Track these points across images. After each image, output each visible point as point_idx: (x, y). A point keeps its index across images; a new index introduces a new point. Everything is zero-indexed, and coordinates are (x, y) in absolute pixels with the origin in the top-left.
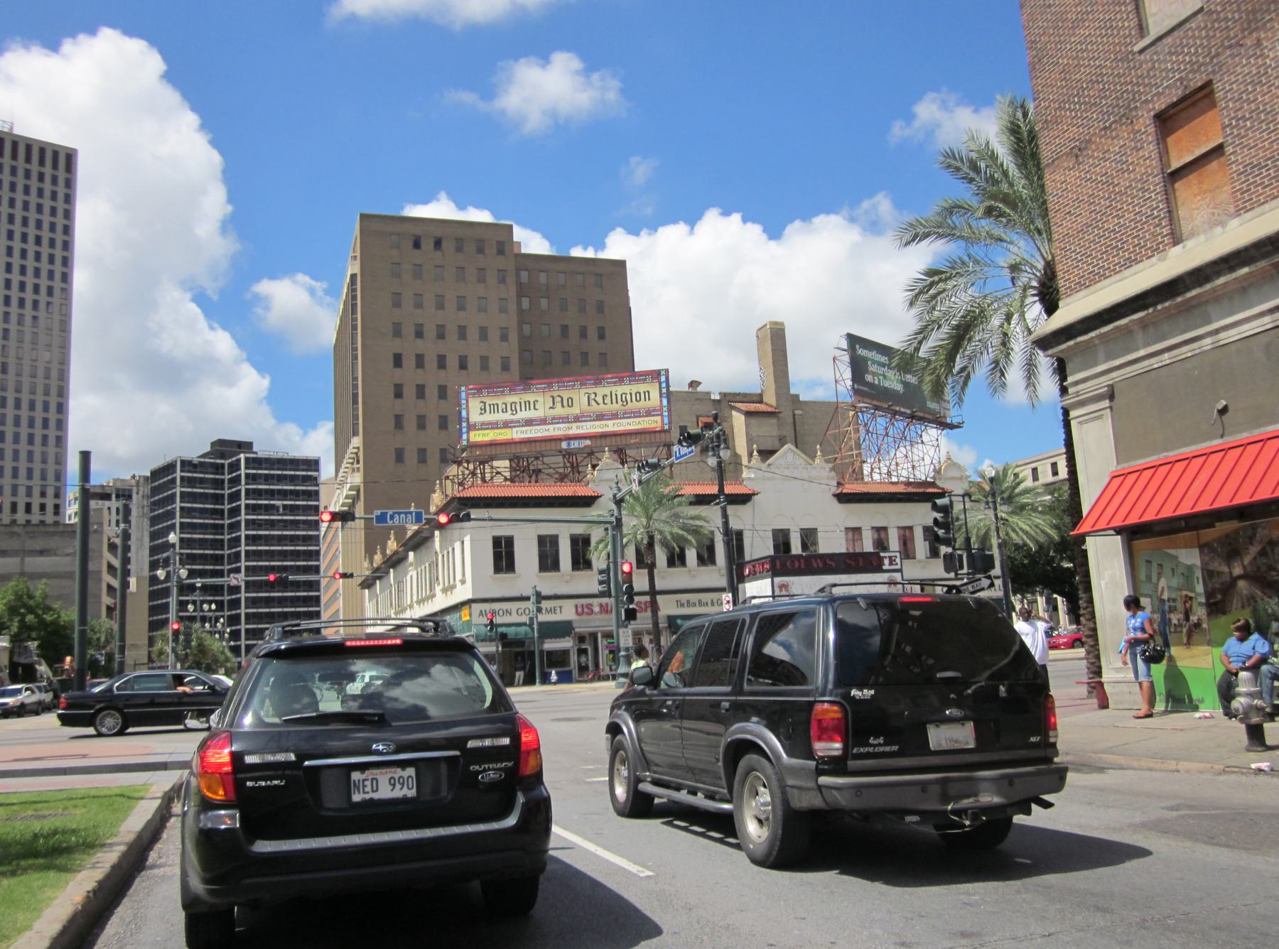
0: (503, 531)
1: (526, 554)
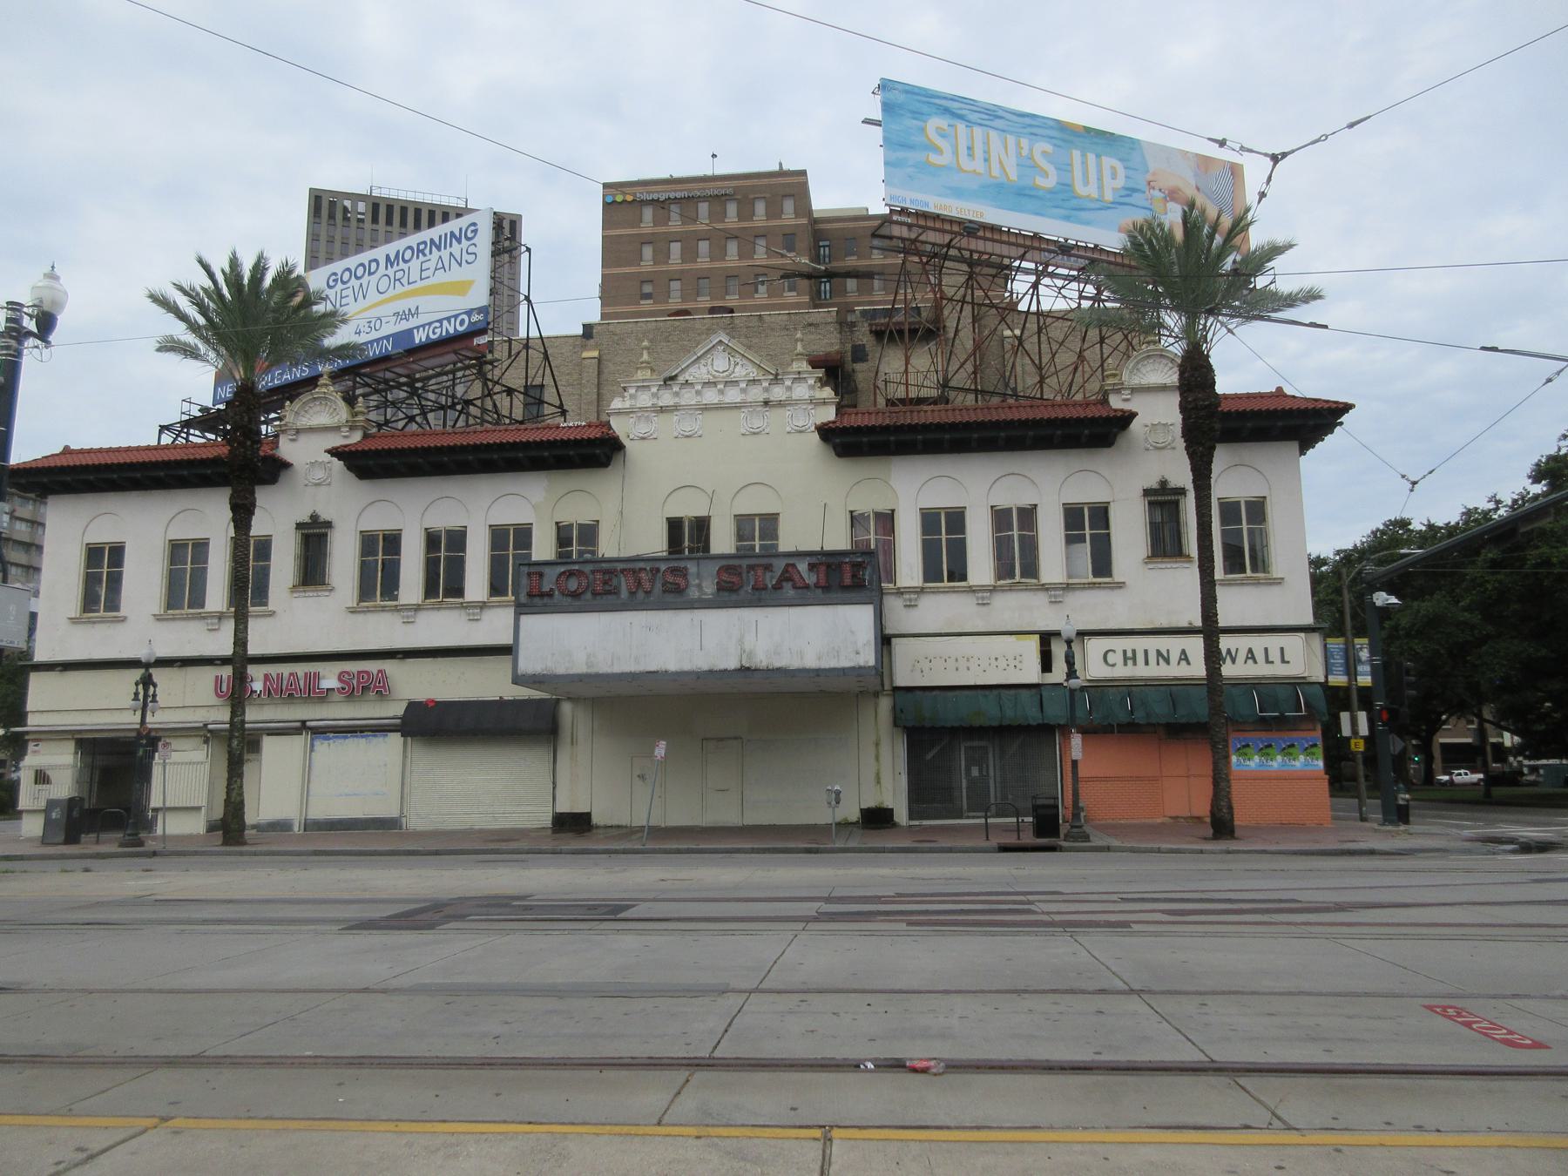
0: (103, 533)
1: (144, 580)
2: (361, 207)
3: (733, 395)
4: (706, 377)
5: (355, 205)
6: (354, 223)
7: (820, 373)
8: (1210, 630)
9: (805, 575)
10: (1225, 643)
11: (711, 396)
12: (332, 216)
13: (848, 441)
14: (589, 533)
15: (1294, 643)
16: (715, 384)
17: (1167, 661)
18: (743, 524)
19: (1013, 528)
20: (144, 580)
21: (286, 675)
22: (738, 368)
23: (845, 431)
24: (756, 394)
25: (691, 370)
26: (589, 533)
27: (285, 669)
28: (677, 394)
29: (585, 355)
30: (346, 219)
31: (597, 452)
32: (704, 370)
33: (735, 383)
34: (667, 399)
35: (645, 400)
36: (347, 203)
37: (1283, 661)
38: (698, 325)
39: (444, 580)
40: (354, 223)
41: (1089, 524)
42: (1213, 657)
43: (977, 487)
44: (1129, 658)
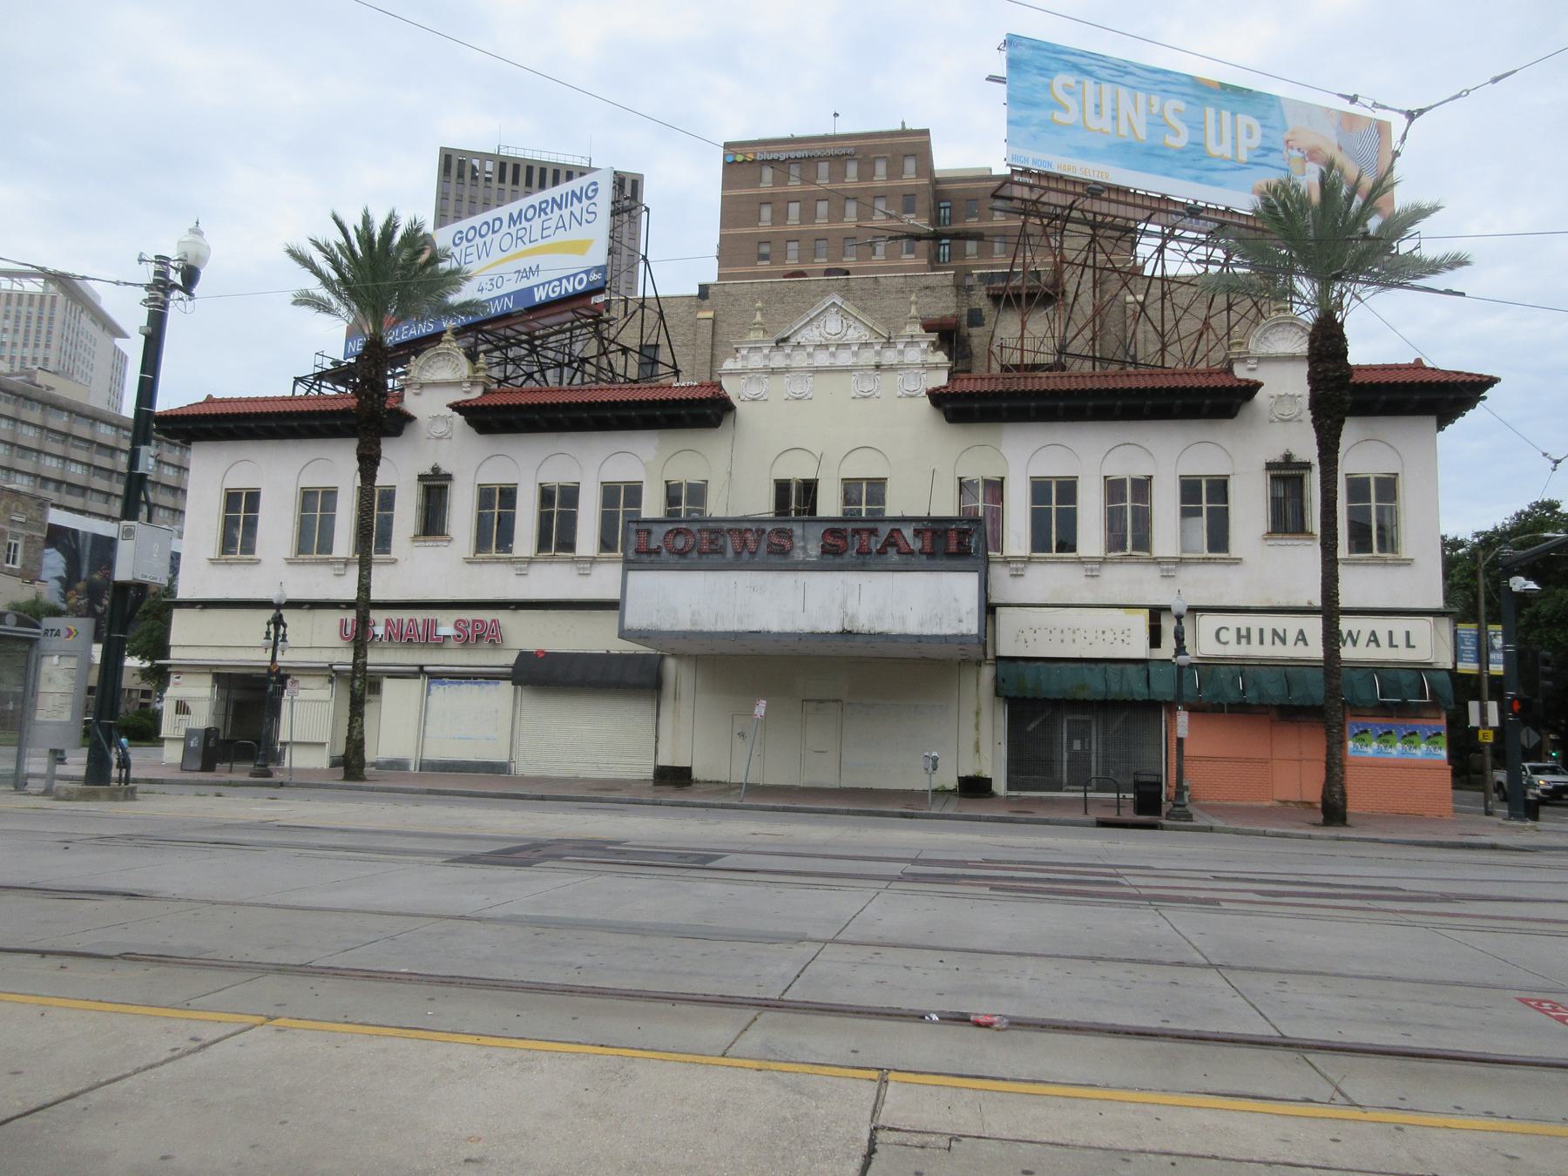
0: (241, 480)
1: (277, 524)
2: (489, 166)
3: (845, 358)
4: (818, 340)
5: (483, 165)
6: (481, 182)
7: (934, 337)
8: (1330, 610)
9: (910, 541)
10: (377, 616)
11: (822, 359)
12: (461, 175)
15: (1421, 628)
16: (827, 346)
17: (1283, 641)
18: (850, 488)
19: (1129, 505)
20: (277, 524)
22: (851, 331)
23: (955, 397)
24: (869, 357)
25: (804, 332)
26: (698, 492)
30: (474, 178)
31: (707, 412)
32: (816, 332)
34: (778, 360)
35: (756, 361)
36: (476, 162)
37: (1408, 645)
38: (813, 286)
41: (1206, 498)
42: (1332, 637)
43: (1091, 456)
44: (1243, 636)
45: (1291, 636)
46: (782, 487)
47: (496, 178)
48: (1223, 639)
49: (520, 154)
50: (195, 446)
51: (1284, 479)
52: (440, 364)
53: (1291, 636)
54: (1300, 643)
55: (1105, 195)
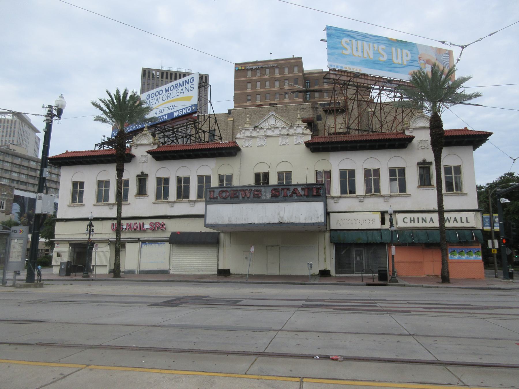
0: (78, 178)
1: (90, 193)
2: (158, 73)
3: (277, 132)
4: (268, 126)
5: (156, 73)
6: (156, 79)
7: (306, 124)
8: (441, 211)
11: (269, 133)
12: (149, 77)
13: (315, 147)
14: (229, 178)
15: (471, 216)
16: (271, 128)
17: (426, 222)
18: (280, 175)
20: (90, 193)
21: (133, 224)
23: (314, 144)
24: (285, 132)
26: (229, 178)
27: (133, 222)
28: (258, 132)
29: (229, 120)
30: (153, 77)
31: (232, 151)
32: (267, 124)
33: (277, 128)
34: (255, 134)
35: (248, 134)
36: (154, 72)
37: (467, 222)
39: (183, 193)
40: (156, 79)
41: (398, 175)
42: (442, 220)
43: (359, 162)
45: (428, 220)
46: (257, 175)
47: (160, 77)
48: (405, 221)
49: (165, 69)
50: (62, 167)
51: (423, 168)
52: (143, 138)
53: (428, 220)
54: (431, 222)
55: (360, 77)
